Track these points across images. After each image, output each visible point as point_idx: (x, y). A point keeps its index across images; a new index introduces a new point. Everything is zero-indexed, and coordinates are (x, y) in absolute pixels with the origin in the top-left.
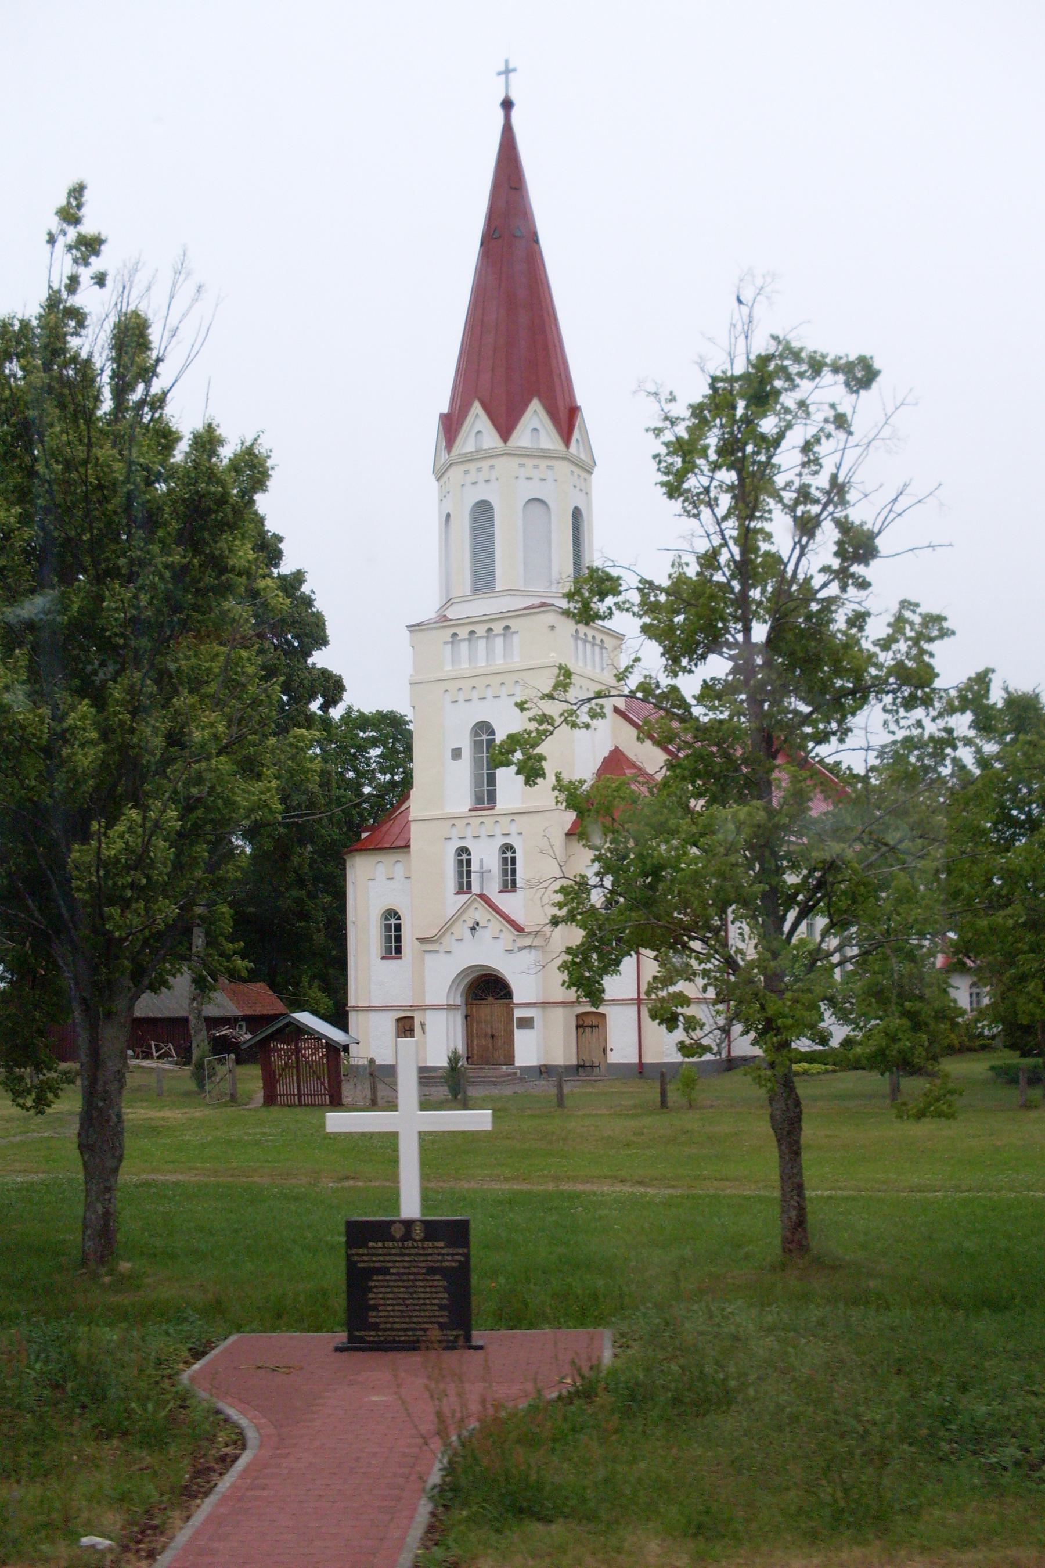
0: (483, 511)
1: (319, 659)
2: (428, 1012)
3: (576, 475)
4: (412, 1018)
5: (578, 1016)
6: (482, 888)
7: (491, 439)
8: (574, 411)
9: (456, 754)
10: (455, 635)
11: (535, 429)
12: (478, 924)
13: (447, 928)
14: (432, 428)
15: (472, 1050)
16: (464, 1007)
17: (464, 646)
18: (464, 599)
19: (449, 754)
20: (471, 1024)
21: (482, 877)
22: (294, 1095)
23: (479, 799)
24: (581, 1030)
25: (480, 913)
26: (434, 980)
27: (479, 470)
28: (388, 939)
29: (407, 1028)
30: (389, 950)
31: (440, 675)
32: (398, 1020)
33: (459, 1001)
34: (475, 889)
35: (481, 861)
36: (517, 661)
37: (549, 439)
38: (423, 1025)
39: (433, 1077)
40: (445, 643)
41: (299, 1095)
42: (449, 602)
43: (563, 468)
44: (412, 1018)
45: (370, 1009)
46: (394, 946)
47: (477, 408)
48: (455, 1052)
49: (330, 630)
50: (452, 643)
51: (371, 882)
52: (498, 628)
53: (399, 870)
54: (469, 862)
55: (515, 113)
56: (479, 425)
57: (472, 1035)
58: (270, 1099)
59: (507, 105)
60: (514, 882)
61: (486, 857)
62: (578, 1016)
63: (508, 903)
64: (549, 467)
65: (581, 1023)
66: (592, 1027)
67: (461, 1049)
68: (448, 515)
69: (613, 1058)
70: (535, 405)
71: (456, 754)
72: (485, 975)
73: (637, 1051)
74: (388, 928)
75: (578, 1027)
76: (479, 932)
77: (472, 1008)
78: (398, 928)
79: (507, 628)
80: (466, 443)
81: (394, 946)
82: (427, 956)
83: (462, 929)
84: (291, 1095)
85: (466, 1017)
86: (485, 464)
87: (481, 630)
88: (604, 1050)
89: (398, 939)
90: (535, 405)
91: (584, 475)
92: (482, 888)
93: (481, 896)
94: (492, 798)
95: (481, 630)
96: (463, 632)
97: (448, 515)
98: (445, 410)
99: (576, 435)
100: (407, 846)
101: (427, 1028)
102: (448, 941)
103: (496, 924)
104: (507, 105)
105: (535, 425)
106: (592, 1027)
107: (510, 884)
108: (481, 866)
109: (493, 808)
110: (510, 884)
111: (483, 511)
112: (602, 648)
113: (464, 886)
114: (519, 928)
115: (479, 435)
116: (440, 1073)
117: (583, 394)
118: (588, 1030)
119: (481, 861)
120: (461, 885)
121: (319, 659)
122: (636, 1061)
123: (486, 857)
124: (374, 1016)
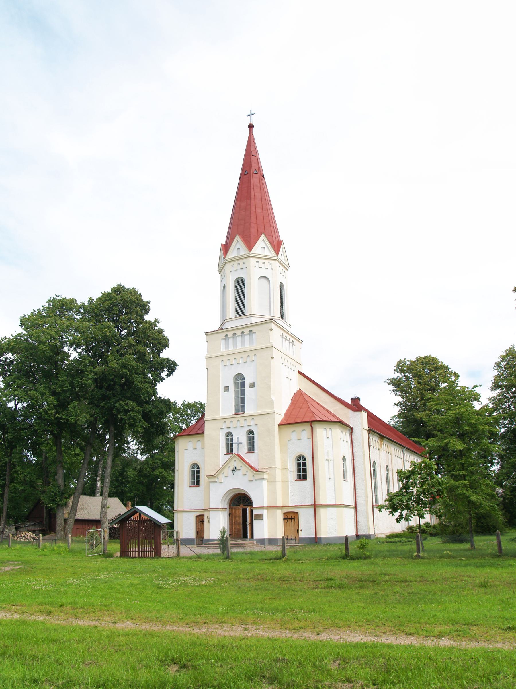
0: (240, 283)
1: (165, 354)
2: (211, 512)
3: (282, 274)
4: (204, 515)
5: (284, 514)
6: (238, 451)
7: (244, 251)
8: (280, 243)
9: (252, 385)
10: (227, 336)
11: (263, 247)
12: (236, 468)
13: (220, 470)
14: (218, 249)
15: (232, 531)
16: (228, 509)
17: (231, 340)
18: (232, 320)
19: (222, 389)
20: (232, 517)
21: (238, 446)
22: (136, 551)
23: (237, 410)
24: (286, 521)
25: (237, 463)
26: (215, 497)
27: (238, 264)
28: (193, 478)
29: (201, 520)
30: (193, 483)
31: (220, 354)
32: (197, 517)
33: (226, 506)
34: (235, 451)
35: (238, 438)
36: (255, 346)
37: (269, 252)
38: (208, 518)
39: (213, 544)
40: (222, 339)
41: (139, 551)
42: (224, 322)
43: (276, 264)
44: (204, 515)
45: (183, 511)
46: (196, 481)
47: (238, 238)
48: (224, 528)
49: (170, 342)
50: (225, 339)
51: (186, 451)
52: (246, 331)
53: (199, 445)
54: (232, 439)
55: (254, 130)
56: (238, 243)
57: (232, 524)
58: (124, 553)
59: (251, 126)
60: (253, 448)
61: (240, 437)
62: (284, 514)
63: (251, 459)
64: (270, 263)
65: (286, 517)
66: (291, 519)
67: (227, 527)
68: (225, 286)
69: (302, 535)
70: (263, 237)
71: (227, 389)
72: (239, 494)
73: (314, 531)
74: (193, 472)
75: (284, 519)
76: (236, 472)
77: (232, 510)
78: (198, 472)
79: (251, 331)
80: (232, 254)
81: (196, 481)
82: (211, 485)
83: (228, 471)
84: (134, 551)
85: (230, 514)
86: (241, 262)
87: (238, 333)
88: (298, 531)
89: (198, 477)
90: (263, 235)
91: (286, 271)
92: (238, 451)
93: (237, 455)
94: (243, 407)
95: (238, 333)
96: (230, 334)
97: (225, 286)
98: (224, 243)
99: (281, 252)
100: (203, 433)
101: (211, 520)
102: (221, 477)
103: (244, 469)
104: (251, 126)
105: (262, 245)
106: (291, 519)
107: (251, 449)
108: (238, 441)
109: (243, 413)
110: (251, 449)
111: (240, 283)
112: (293, 345)
113: (230, 451)
114: (256, 470)
115: (239, 250)
116: (216, 542)
117: (284, 233)
118: (289, 521)
119: (238, 438)
120: (228, 450)
121: (165, 354)
122: (314, 536)
123: (240, 437)
124: (185, 515)
